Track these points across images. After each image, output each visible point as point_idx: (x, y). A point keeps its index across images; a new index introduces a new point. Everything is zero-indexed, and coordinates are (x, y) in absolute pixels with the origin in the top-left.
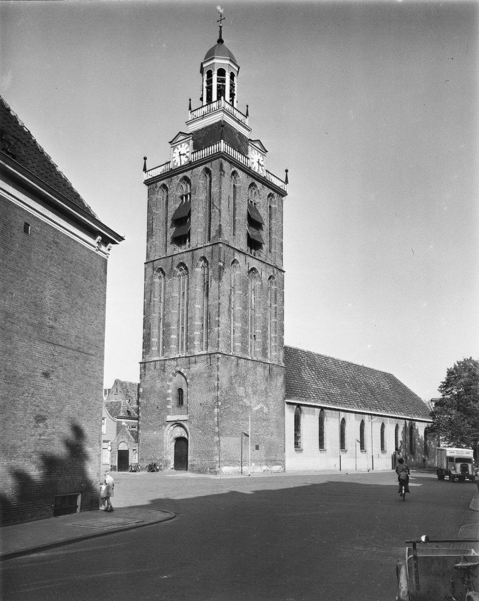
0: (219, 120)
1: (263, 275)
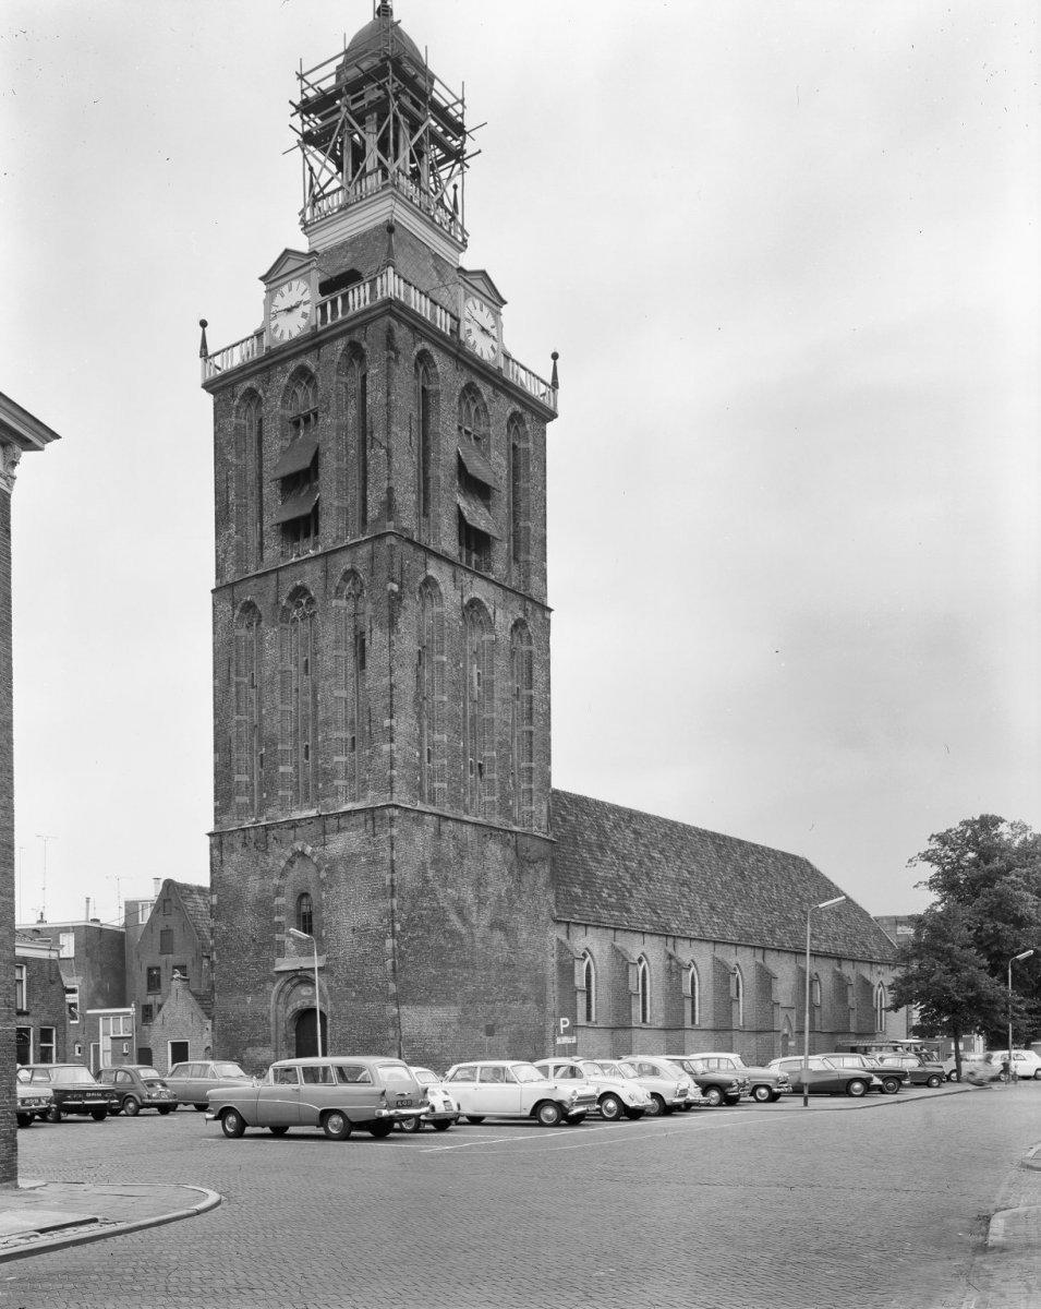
0: (385, 218)
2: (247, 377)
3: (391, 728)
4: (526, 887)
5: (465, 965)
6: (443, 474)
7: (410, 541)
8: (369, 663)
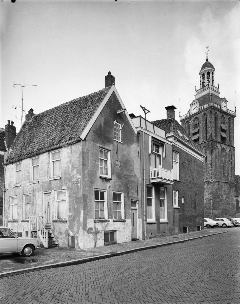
0: (208, 92)
1: (227, 150)
2: (187, 119)
3: (212, 169)
4: (231, 191)
5: (222, 204)
6: (219, 129)
7: (214, 141)
8: (208, 160)
